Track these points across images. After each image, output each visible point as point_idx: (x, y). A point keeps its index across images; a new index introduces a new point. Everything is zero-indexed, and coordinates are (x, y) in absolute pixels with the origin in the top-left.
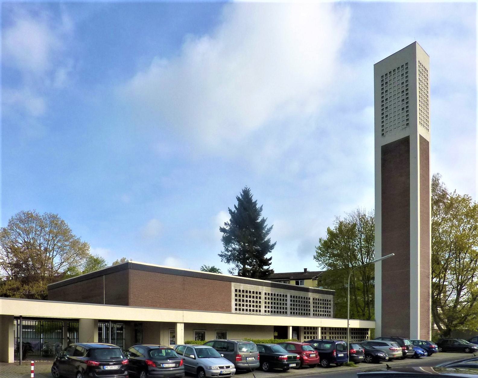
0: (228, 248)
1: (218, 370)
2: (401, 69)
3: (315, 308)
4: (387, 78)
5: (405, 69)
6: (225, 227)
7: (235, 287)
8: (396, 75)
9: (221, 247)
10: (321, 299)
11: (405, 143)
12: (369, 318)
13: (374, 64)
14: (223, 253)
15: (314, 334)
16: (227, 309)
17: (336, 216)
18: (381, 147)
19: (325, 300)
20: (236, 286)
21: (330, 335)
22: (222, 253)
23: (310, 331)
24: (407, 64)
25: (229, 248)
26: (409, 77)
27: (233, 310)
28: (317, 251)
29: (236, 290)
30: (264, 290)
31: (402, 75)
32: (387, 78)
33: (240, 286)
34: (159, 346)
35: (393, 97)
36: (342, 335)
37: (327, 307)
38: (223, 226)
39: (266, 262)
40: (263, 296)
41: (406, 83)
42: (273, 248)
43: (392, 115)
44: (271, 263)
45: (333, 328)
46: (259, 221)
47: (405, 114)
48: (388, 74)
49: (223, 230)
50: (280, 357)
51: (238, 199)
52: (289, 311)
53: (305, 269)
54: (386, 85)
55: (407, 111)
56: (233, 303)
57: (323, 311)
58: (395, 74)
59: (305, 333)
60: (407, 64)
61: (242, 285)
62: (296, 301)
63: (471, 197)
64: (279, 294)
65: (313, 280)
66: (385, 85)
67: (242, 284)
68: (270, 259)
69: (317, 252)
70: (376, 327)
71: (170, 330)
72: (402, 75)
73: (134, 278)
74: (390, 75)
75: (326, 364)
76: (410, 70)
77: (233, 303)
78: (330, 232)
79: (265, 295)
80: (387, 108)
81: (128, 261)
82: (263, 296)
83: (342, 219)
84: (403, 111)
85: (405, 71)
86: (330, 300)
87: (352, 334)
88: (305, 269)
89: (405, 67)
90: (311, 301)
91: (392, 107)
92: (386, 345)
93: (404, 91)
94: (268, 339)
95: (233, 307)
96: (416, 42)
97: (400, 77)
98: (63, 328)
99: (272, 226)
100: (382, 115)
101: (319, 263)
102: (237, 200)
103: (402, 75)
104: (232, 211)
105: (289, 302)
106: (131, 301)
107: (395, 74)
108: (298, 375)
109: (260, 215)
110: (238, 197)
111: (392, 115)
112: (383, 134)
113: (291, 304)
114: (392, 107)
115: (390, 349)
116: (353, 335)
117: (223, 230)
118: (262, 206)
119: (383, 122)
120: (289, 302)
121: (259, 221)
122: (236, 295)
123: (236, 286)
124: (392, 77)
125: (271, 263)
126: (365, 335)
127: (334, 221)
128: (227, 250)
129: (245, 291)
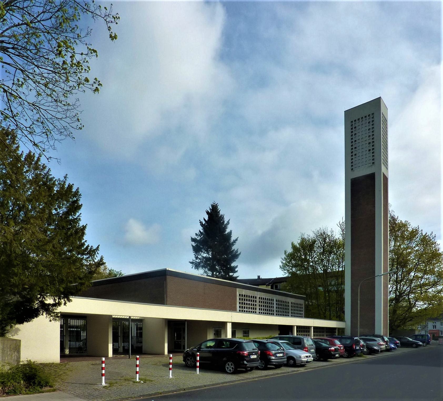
0: (198, 256)
1: (305, 358)
2: (368, 117)
3: (281, 309)
4: (356, 123)
5: (371, 118)
6: (196, 237)
7: (239, 292)
8: (364, 122)
9: (191, 256)
10: (295, 303)
11: (371, 178)
12: (340, 318)
13: (345, 110)
14: (194, 261)
17: (302, 232)
18: (350, 180)
19: (299, 304)
22: (193, 261)
24: (373, 114)
25: (198, 256)
28: (282, 261)
29: (240, 295)
30: (258, 295)
31: (369, 122)
32: (356, 123)
34: (267, 340)
35: (361, 139)
36: (306, 333)
38: (194, 236)
39: (233, 270)
40: (258, 300)
41: (372, 129)
42: (238, 258)
43: (360, 154)
44: (237, 271)
46: (226, 233)
47: (371, 155)
48: (357, 120)
49: (193, 240)
50: (330, 349)
51: (208, 213)
52: (275, 314)
53: (259, 277)
54: (355, 130)
55: (373, 153)
56: (238, 305)
58: (363, 121)
60: (373, 114)
61: (244, 290)
62: (249, 304)
63: (410, 223)
64: (269, 298)
65: (266, 286)
66: (354, 129)
68: (237, 267)
69: (282, 262)
70: (346, 326)
71: (214, 328)
72: (369, 122)
73: (171, 282)
74: (358, 121)
75: (347, 355)
76: (375, 119)
77: (238, 305)
78: (294, 247)
79: (239, 300)
80: (355, 148)
81: (166, 268)
82: (258, 300)
83: (306, 237)
84: (370, 152)
85: (371, 120)
86: (302, 304)
87: (315, 332)
88: (259, 277)
89: (371, 116)
90: (290, 305)
91: (361, 147)
92: (375, 341)
93: (370, 136)
94: (262, 337)
96: (380, 97)
97: (367, 124)
98: (119, 326)
99: (238, 238)
100: (351, 154)
101: (284, 272)
102: (206, 213)
103: (369, 122)
104: (202, 223)
105: (275, 306)
107: (363, 121)
108: (339, 364)
109: (227, 228)
110: (207, 211)
111: (360, 154)
112: (352, 169)
114: (361, 147)
115: (378, 343)
116: (315, 334)
117: (193, 240)
118: (229, 220)
119: (352, 159)
120: (275, 306)
121: (226, 233)
122: (240, 299)
124: (360, 123)
125: (237, 271)
126: (325, 332)
127: (300, 237)
128: (197, 258)
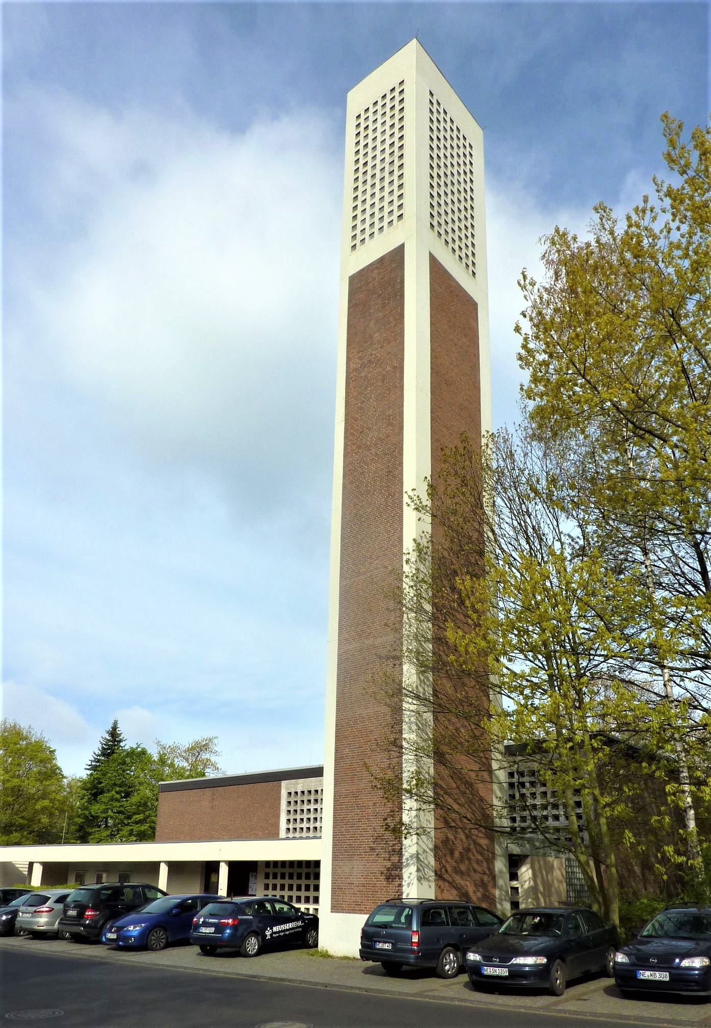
7: (287, 788)
15: (292, 879)
16: (273, 835)
20: (289, 786)
21: (267, 881)
23: (279, 870)
26: (451, 254)
27: (283, 834)
33: (296, 784)
37: (291, 823)
45: (276, 863)
56: (283, 817)
57: (295, 829)
59: (267, 876)
67: (300, 781)
95: (283, 825)
106: (162, 822)
113: (289, 820)
123: (289, 786)
129: (306, 792)
